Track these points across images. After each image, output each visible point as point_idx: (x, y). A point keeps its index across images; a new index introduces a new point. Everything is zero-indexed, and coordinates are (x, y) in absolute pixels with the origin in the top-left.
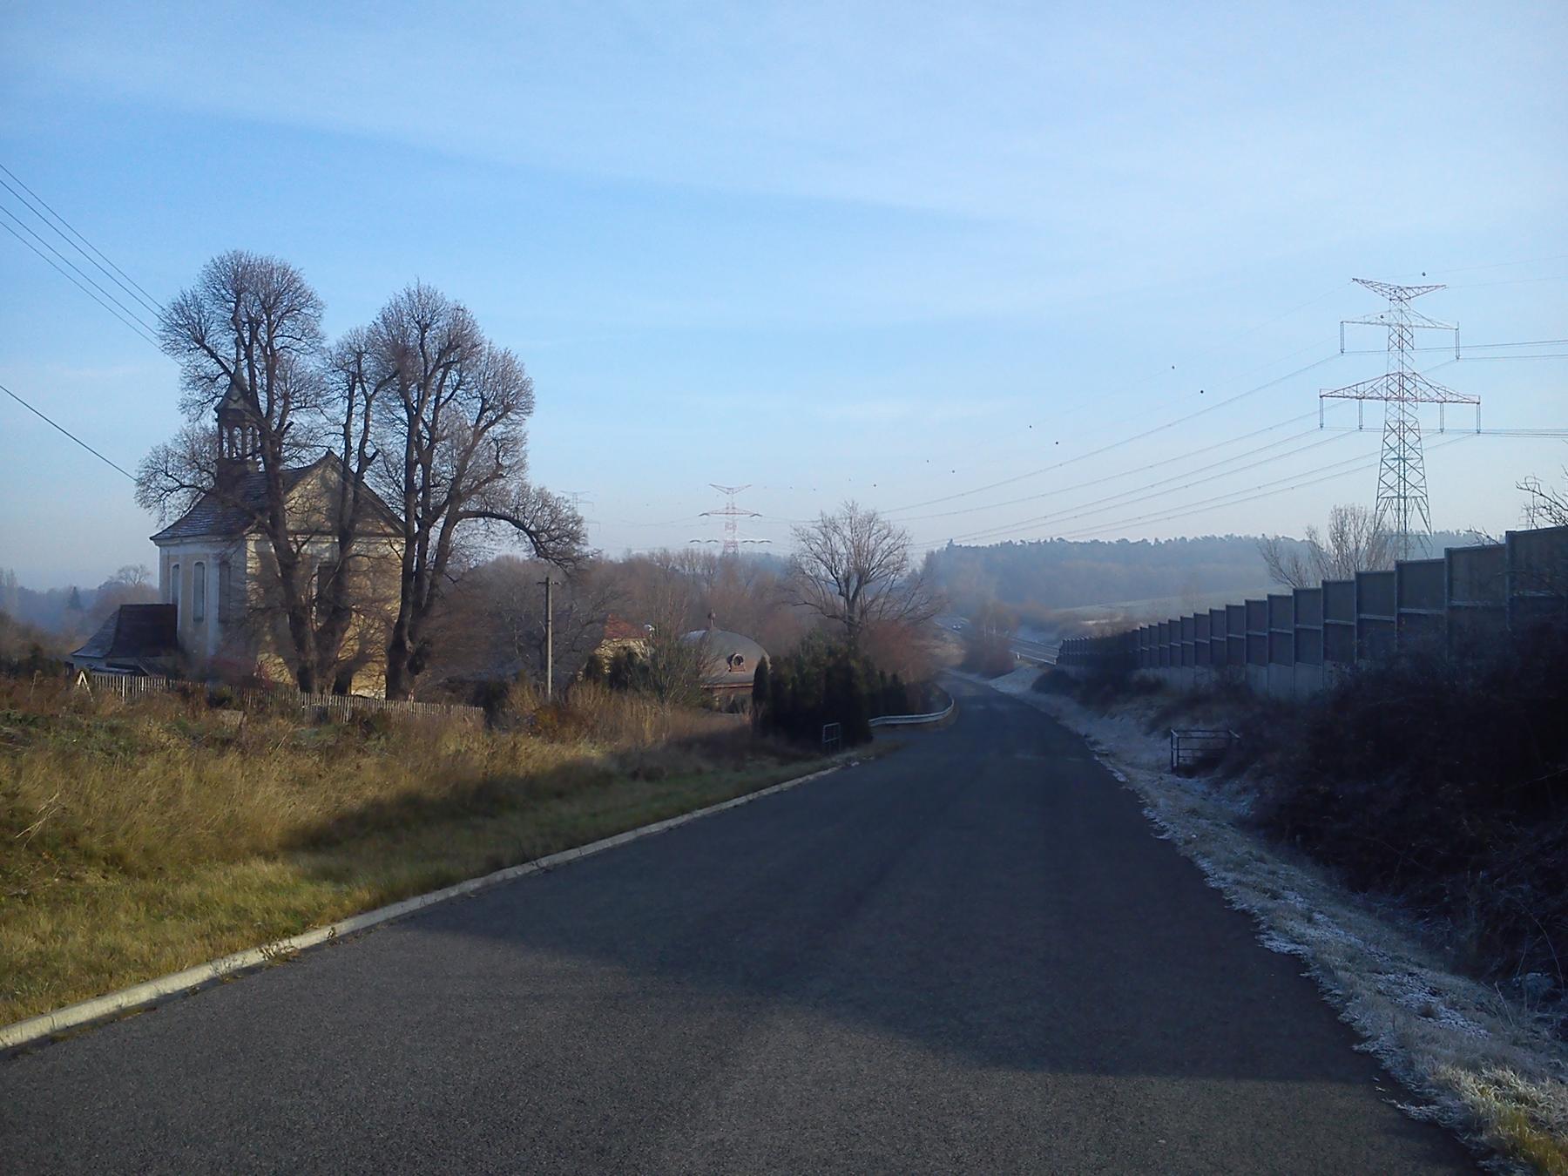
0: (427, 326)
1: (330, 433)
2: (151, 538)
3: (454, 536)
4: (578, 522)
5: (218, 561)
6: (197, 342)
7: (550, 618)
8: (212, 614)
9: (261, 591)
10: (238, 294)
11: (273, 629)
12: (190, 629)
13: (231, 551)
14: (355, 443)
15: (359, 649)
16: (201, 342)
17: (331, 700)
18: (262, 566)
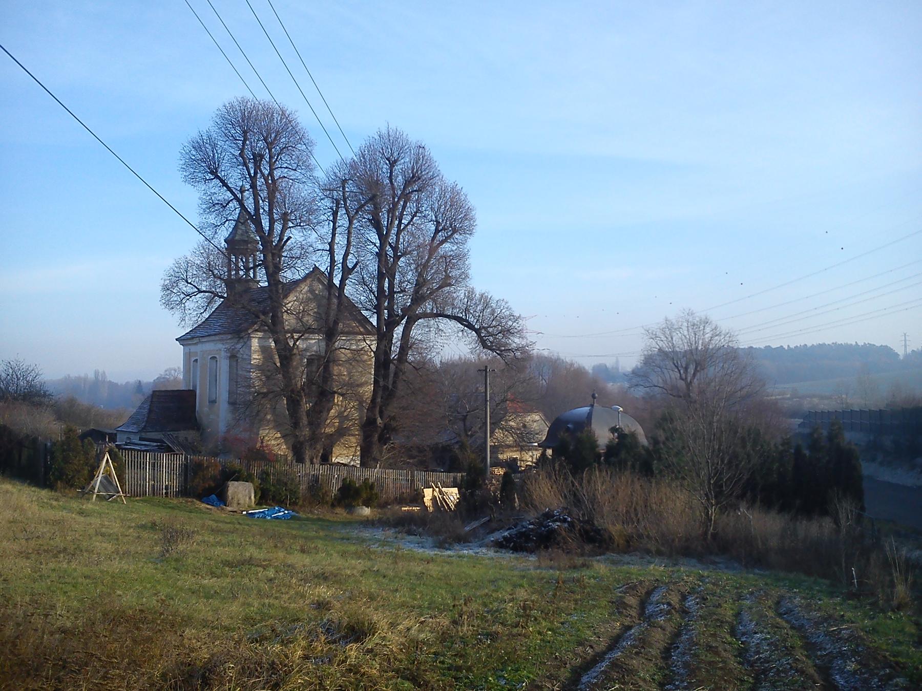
0: (395, 161)
1: (318, 250)
2: (177, 340)
3: (413, 333)
4: (516, 319)
5: (229, 355)
6: (212, 173)
7: (488, 399)
8: (223, 395)
9: (264, 378)
10: (245, 132)
11: (274, 409)
12: (206, 409)
13: (239, 346)
14: (339, 258)
15: (339, 426)
16: (214, 173)
17: (320, 470)
18: (264, 358)
